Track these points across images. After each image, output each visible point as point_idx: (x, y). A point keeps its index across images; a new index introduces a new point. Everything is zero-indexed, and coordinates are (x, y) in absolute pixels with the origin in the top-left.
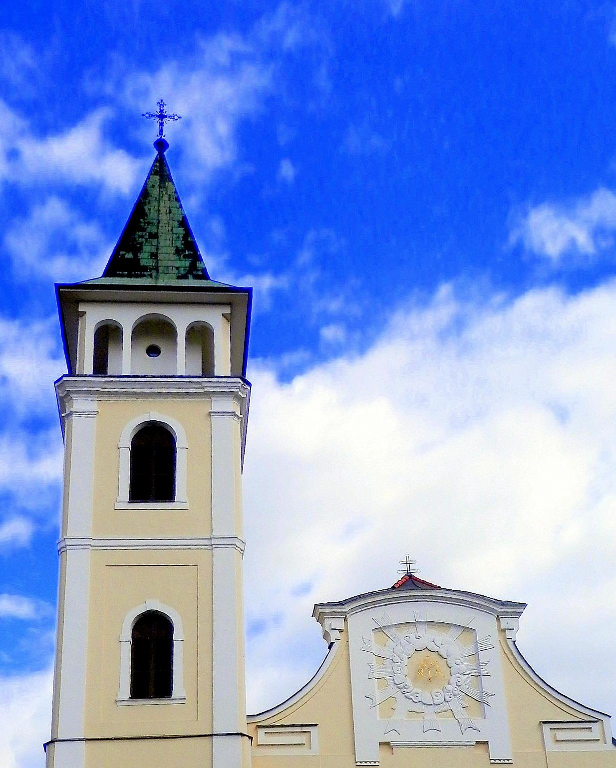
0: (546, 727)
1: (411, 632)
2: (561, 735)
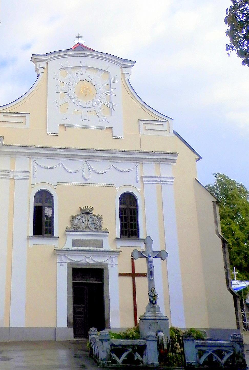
0: (141, 123)
1: (79, 71)
2: (148, 127)
